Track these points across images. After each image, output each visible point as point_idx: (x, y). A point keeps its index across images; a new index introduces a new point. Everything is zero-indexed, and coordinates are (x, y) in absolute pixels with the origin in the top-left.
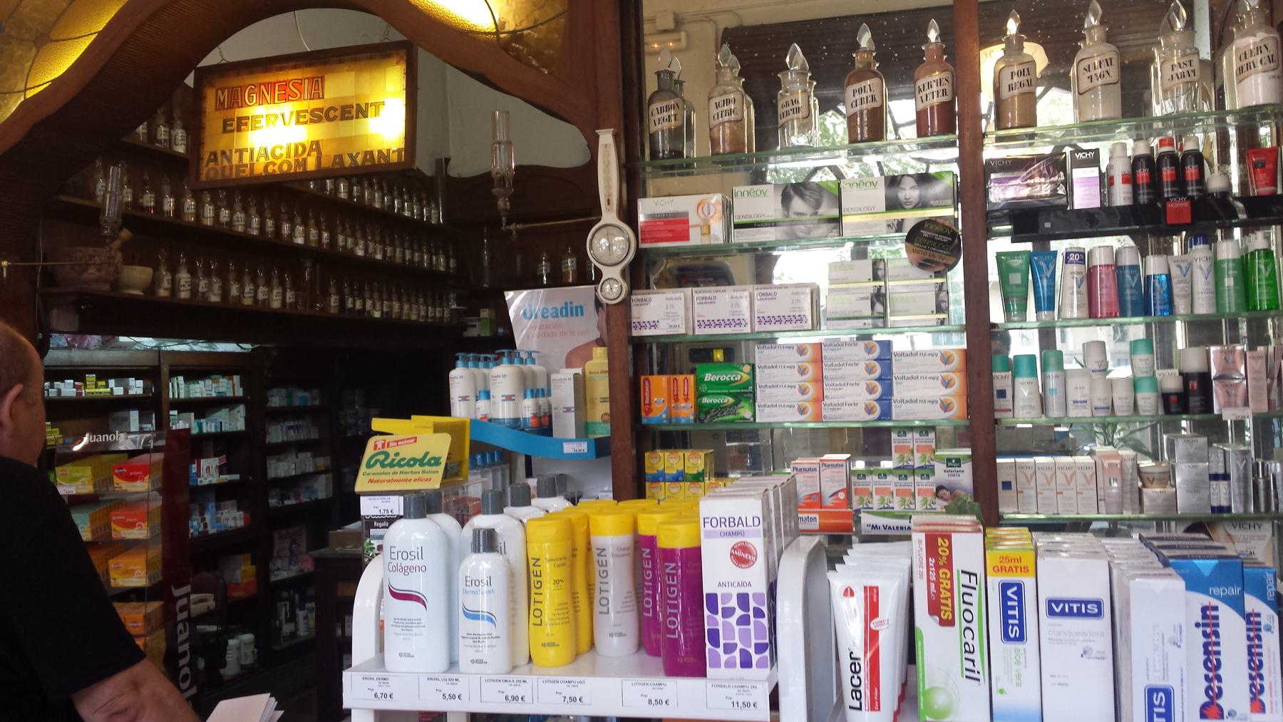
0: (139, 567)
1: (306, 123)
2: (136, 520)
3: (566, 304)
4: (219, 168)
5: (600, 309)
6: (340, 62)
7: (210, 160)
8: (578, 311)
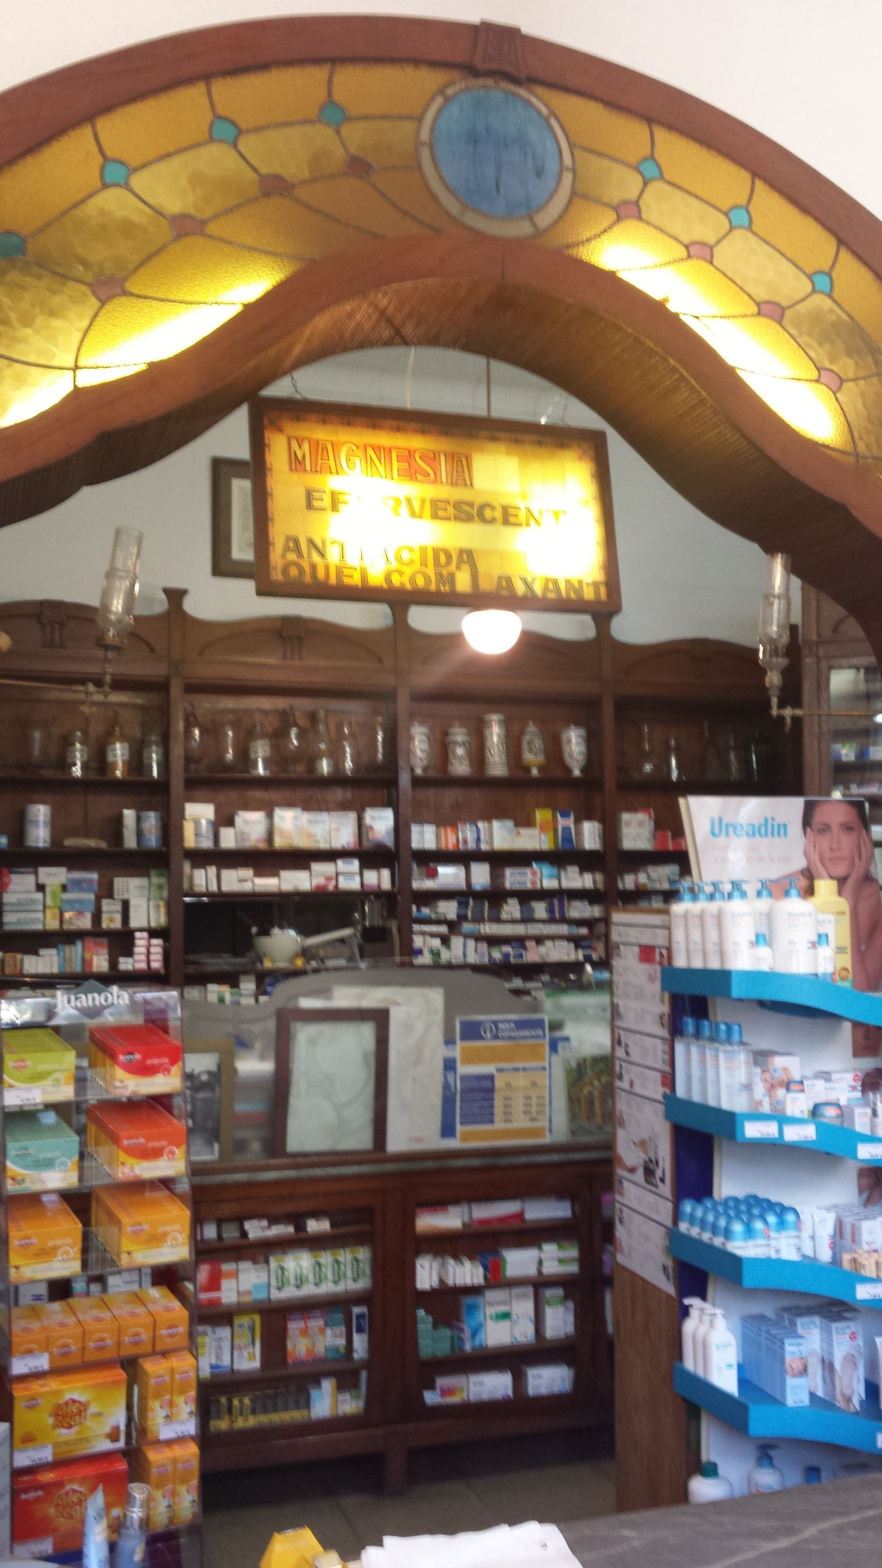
0: (70, 1240)
1: (448, 519)
2: (58, 1154)
3: (766, 820)
5: (808, 829)
6: (494, 439)
7: (286, 549)
8: (782, 830)
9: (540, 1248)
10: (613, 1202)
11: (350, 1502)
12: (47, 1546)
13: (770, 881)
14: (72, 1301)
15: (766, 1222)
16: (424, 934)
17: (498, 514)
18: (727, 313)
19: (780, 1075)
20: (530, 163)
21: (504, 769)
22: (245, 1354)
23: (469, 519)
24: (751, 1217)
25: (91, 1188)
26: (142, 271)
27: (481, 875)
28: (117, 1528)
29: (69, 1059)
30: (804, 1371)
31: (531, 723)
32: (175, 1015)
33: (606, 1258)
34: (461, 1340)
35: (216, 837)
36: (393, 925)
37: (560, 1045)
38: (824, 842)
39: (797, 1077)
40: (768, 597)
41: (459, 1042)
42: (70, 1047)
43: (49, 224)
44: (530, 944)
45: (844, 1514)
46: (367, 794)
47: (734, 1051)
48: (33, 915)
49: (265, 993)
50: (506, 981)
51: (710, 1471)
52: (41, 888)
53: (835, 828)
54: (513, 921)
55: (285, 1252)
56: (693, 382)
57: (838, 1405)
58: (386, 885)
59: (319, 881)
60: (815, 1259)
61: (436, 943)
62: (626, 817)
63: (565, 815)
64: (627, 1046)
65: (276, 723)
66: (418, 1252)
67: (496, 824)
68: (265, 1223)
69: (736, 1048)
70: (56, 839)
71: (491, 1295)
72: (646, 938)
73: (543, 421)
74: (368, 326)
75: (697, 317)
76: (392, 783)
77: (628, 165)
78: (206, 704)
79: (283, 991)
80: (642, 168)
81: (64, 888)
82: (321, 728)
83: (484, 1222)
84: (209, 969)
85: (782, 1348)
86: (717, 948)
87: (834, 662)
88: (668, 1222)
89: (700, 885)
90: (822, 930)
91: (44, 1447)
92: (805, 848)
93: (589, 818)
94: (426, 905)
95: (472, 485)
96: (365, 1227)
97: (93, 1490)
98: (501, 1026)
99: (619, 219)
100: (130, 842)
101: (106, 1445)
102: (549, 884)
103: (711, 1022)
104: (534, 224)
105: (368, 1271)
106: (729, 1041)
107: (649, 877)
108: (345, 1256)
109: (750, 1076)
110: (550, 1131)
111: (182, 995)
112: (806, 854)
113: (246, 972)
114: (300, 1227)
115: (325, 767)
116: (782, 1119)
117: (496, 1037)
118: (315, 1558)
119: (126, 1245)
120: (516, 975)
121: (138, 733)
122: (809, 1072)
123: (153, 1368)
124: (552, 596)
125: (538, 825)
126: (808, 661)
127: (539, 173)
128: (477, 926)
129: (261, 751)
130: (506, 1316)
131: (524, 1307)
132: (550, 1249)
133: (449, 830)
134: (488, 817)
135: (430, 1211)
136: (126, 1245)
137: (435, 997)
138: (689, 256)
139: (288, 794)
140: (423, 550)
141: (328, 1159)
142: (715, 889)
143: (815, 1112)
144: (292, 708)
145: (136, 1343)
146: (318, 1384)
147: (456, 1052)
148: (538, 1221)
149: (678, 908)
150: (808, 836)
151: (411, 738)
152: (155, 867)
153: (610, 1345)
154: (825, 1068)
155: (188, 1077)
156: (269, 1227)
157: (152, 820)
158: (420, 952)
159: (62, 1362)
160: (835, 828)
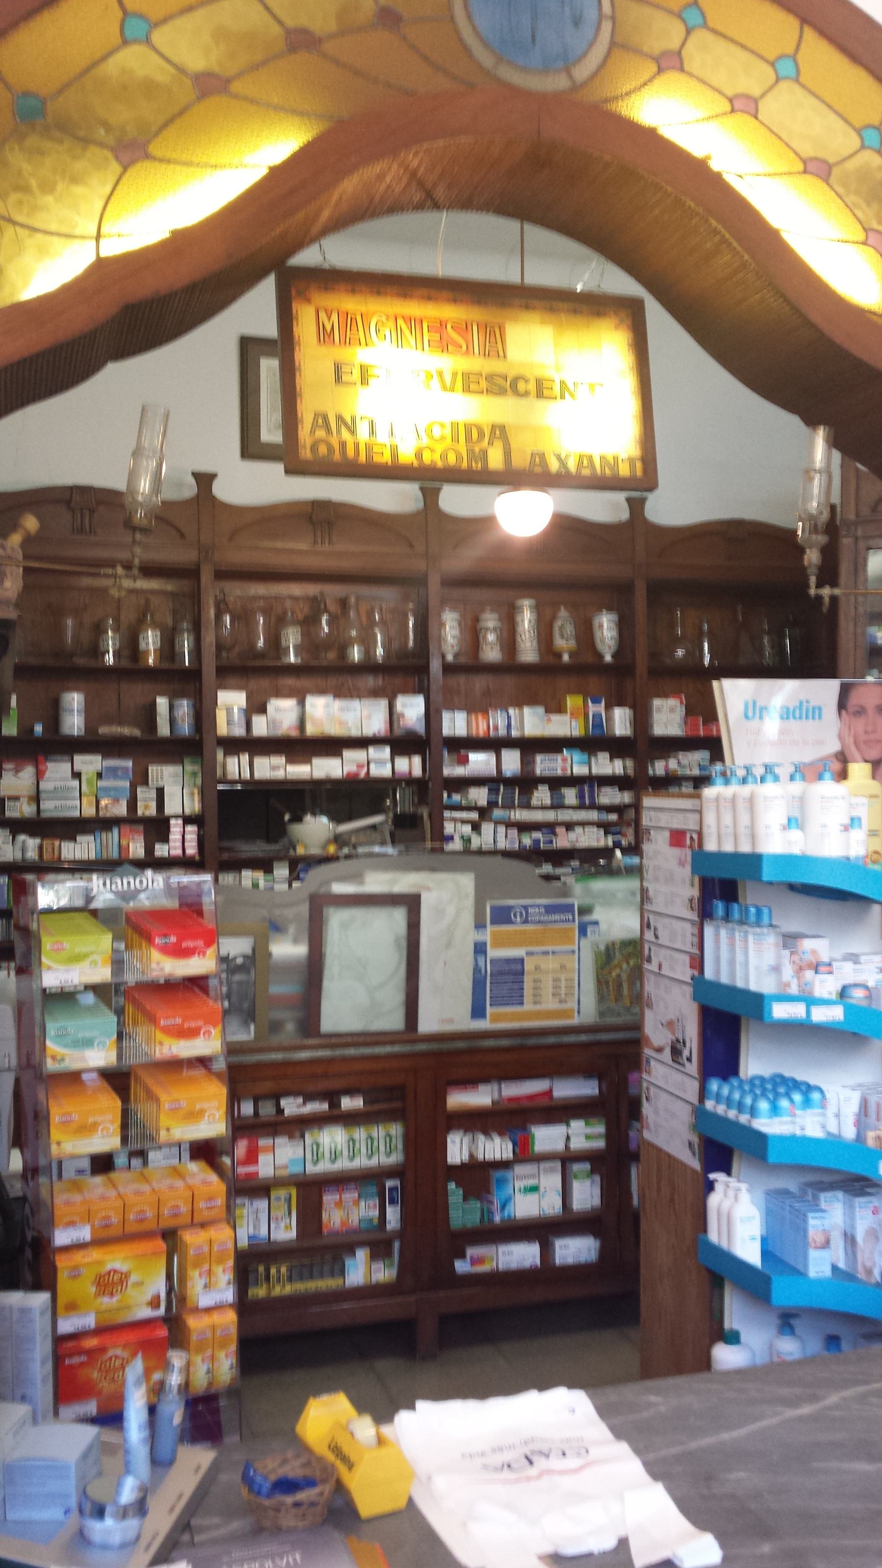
3: (801, 703)
4: (334, 441)
6: (527, 307)
8: (816, 713)
9: (568, 1125)
10: (640, 1081)
11: (384, 1365)
12: (91, 1407)
13: (804, 764)
14: (114, 1175)
15: (792, 1101)
16: (454, 820)
17: (532, 387)
18: (772, 171)
19: (808, 957)
20: (567, 10)
21: (536, 655)
22: (282, 1225)
23: (502, 392)
24: (777, 1095)
25: (130, 1066)
26: (165, 133)
27: (511, 762)
28: (158, 1390)
29: (105, 941)
30: (826, 1244)
31: (562, 608)
32: (209, 900)
33: (632, 1134)
34: (490, 1212)
35: (249, 725)
36: (425, 812)
37: (589, 930)
38: (860, 724)
39: (825, 959)
40: (808, 473)
41: (489, 928)
42: (105, 929)
43: (67, 86)
44: (560, 830)
45: (866, 1382)
46: (398, 681)
47: (763, 934)
48: (70, 803)
49: (298, 878)
50: (537, 866)
51: (733, 1338)
52: (77, 775)
53: (871, 711)
54: (543, 808)
55: (320, 1128)
56: (735, 244)
57: (859, 1276)
58: (417, 772)
59: (350, 768)
60: (840, 1136)
61: (467, 829)
62: (657, 702)
63: (596, 701)
64: (655, 929)
65: (306, 610)
66: (449, 1128)
67: (527, 710)
68: (300, 1100)
69: (765, 930)
70: (90, 725)
71: (519, 1169)
72: (677, 823)
73: (579, 288)
74: (398, 189)
75: (740, 176)
76: (423, 669)
77: (670, 12)
78: (237, 591)
79: (315, 877)
80: (684, 16)
81: (100, 775)
82: (352, 614)
83: (511, 1100)
84: (244, 856)
85: (805, 1221)
86: (748, 832)
87: (872, 543)
88: (695, 1100)
89: (733, 770)
90: (855, 814)
91: (86, 1314)
92: (840, 730)
93: (620, 705)
94: (457, 791)
95: (505, 356)
96: (398, 1104)
97: (134, 1355)
98: (530, 910)
99: (660, 71)
100: (164, 729)
101: (146, 1313)
102: (580, 770)
103: (741, 906)
104: (570, 77)
105: (400, 1146)
106: (758, 924)
107: (679, 763)
108: (379, 1132)
109: (779, 957)
110: (579, 1012)
111: (216, 880)
112: (840, 737)
113: (280, 859)
114: (335, 1104)
115: (356, 654)
116: (810, 1001)
117: (526, 921)
118: (348, 1422)
119: (164, 1121)
120: (546, 861)
121: (169, 621)
122: (838, 955)
123: (192, 1239)
124: (586, 472)
125: (568, 711)
126: (846, 542)
127: (577, 22)
128: (508, 812)
129: (292, 637)
130: (534, 1189)
131: (552, 1181)
132: (577, 1126)
133: (480, 717)
134: (519, 704)
135: (459, 1089)
136: (164, 1121)
137: (466, 882)
138: (733, 111)
139: (320, 681)
140: (455, 426)
141: (361, 1039)
142: (748, 773)
143: (843, 993)
144: (322, 594)
145: (176, 1215)
146: (353, 1254)
147: (487, 936)
148: (565, 1099)
149: (709, 792)
150: (843, 719)
151: (442, 625)
152: (189, 754)
153: (636, 1218)
154: (854, 951)
155: (224, 960)
156: (304, 1103)
157: (184, 707)
158: (451, 838)
159: (103, 1234)
160: (871, 711)
